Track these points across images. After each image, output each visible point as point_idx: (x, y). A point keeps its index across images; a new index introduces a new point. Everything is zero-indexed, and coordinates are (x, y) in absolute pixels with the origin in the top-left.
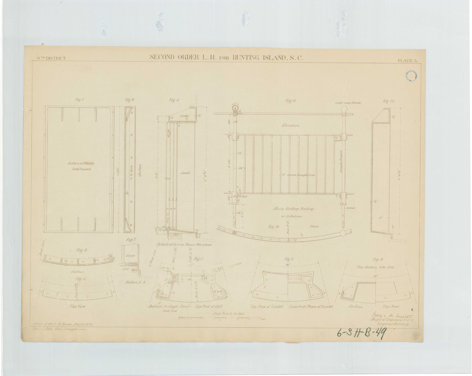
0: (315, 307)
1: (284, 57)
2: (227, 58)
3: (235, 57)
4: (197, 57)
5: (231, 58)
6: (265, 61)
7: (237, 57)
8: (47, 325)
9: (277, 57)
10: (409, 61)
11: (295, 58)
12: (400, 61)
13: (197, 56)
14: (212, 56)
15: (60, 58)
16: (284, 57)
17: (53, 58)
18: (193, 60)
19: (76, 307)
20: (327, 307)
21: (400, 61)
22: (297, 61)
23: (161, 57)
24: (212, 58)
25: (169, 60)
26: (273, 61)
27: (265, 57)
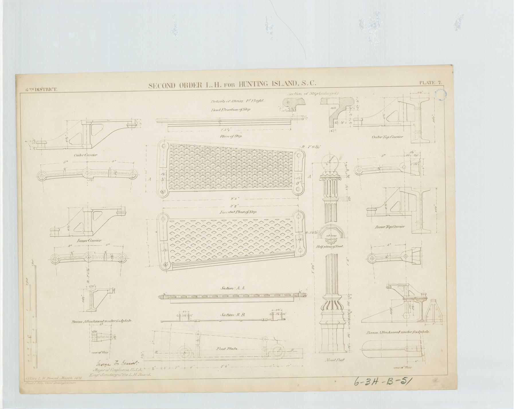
3: (241, 83)
4: (200, 85)
5: (237, 86)
6: (274, 87)
7: (243, 84)
10: (432, 83)
12: (422, 83)
13: (200, 84)
14: (217, 83)
15: (50, 89)
18: (186, 88)
19: (388, 137)
21: (422, 83)
22: (310, 86)
23: (160, 86)
24: (217, 86)
25: (169, 89)
26: (283, 87)
27: (274, 84)
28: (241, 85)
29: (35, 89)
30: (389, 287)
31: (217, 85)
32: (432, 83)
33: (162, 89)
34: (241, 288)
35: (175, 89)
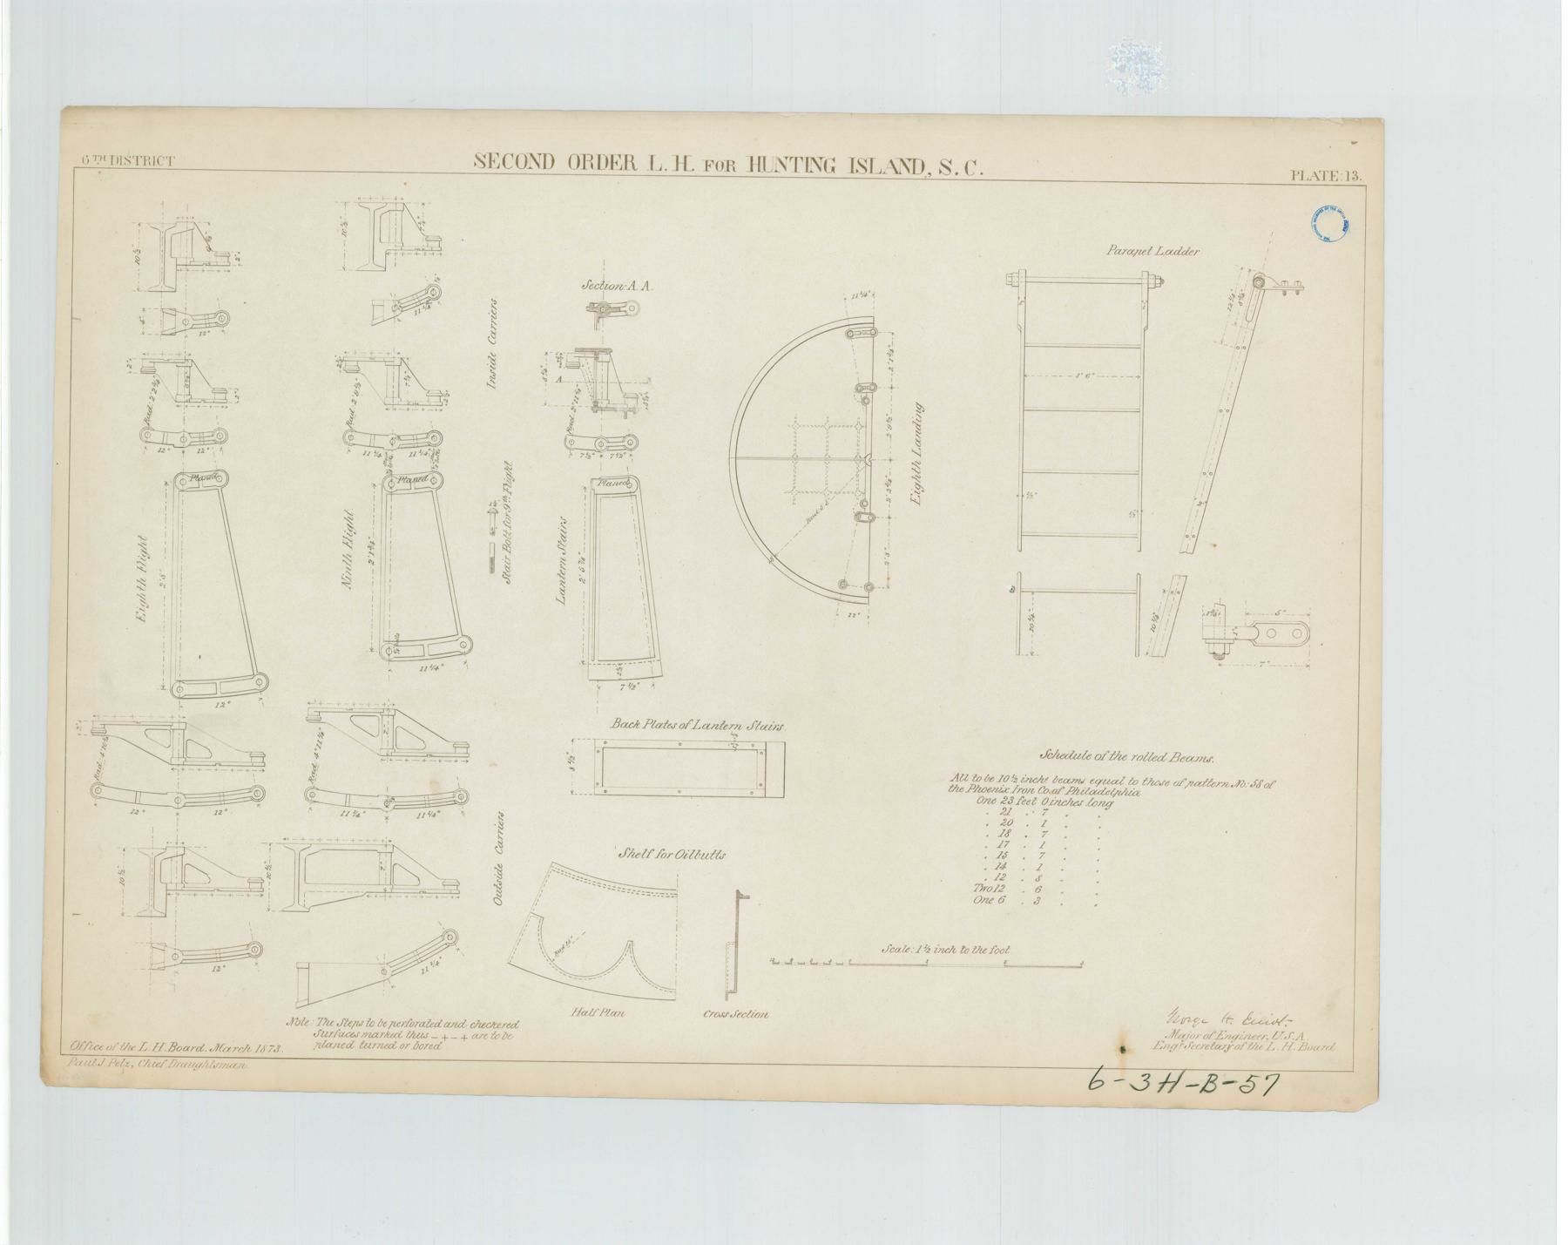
0: (1225, 784)
1: (918, 164)
2: (728, 165)
3: (755, 161)
4: (629, 162)
5: (743, 166)
8: (118, 1051)
9: (898, 164)
10: (1328, 176)
11: (958, 166)
12: (1298, 177)
14: (681, 160)
16: (918, 164)
17: (134, 161)
20: (562, 583)
21: (1298, 177)
24: (681, 166)
27: (856, 166)
28: (755, 168)
29: (108, 159)
30: (443, 396)
31: (682, 162)
32: (1328, 176)
33: (515, 169)
34: (640, 284)
35: (554, 170)
